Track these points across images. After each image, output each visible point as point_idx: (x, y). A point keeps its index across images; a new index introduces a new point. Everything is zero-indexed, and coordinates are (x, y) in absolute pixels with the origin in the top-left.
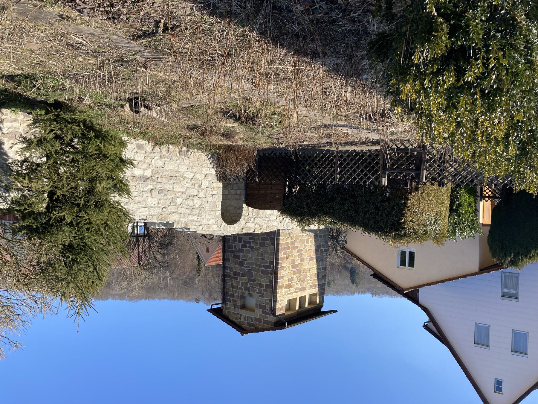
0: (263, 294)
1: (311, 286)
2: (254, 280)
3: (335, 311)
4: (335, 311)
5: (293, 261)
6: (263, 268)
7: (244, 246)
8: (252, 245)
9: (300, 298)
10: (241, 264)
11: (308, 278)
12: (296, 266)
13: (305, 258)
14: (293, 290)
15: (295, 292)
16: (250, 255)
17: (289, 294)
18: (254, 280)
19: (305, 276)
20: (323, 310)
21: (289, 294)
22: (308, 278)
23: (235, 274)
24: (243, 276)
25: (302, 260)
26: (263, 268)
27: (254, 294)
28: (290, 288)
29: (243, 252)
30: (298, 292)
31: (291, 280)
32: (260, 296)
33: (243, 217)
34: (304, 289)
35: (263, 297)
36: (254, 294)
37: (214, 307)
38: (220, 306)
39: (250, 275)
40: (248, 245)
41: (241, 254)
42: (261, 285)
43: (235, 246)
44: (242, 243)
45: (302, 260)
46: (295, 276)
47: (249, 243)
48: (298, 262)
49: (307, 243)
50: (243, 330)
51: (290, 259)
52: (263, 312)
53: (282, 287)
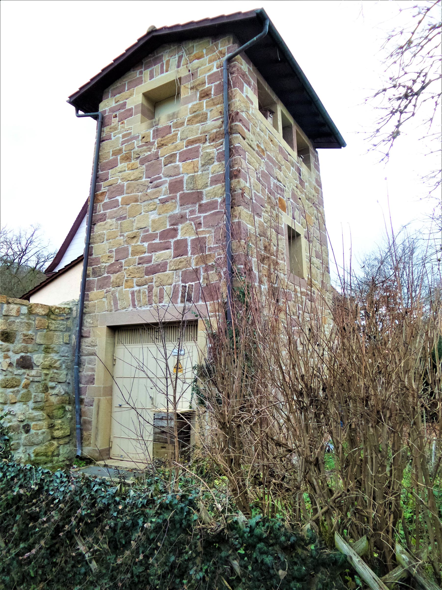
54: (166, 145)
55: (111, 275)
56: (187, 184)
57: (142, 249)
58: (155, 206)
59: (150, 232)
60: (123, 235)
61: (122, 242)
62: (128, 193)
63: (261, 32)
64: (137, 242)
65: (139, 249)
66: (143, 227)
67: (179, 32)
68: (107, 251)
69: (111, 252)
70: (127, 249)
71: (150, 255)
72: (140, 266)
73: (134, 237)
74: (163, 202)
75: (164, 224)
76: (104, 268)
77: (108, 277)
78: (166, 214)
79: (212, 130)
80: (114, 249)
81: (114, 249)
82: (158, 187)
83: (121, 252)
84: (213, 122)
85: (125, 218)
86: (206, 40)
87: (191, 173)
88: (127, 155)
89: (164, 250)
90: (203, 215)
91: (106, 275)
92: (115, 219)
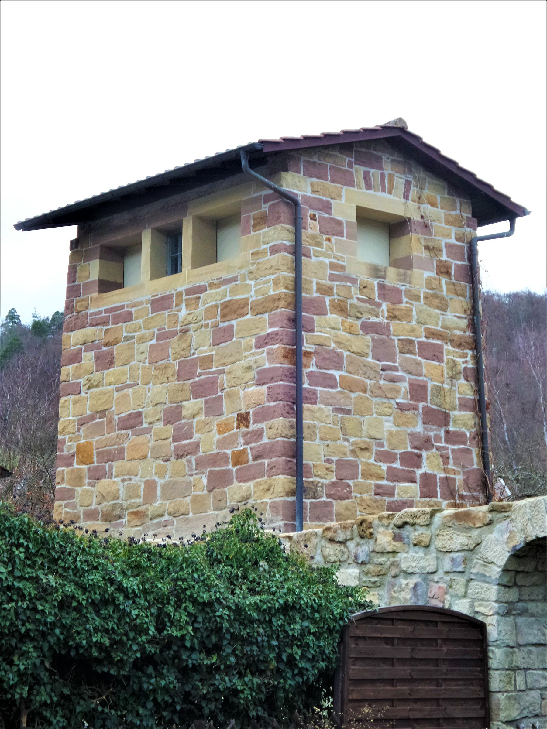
0: (332, 278)
1: (128, 317)
2: (367, 328)
3: (29, 225)
4: (29, 225)
5: (213, 408)
6: (337, 374)
7: (413, 460)
8: (384, 467)
9: (175, 267)
10: (418, 391)
11: (145, 347)
12: (198, 391)
13: (159, 425)
14: (211, 298)
15: (201, 289)
16: (388, 425)
17: (227, 281)
18: (367, 328)
19: (157, 354)
20: (71, 232)
21: (227, 281)
22: (145, 347)
23: (435, 354)
24: (407, 346)
25: (173, 416)
26: (337, 374)
27: (364, 277)
28: (226, 305)
29: (413, 435)
30: (189, 292)
31: (222, 336)
32: (343, 268)
33: (495, 572)
34: (161, 303)
35: (333, 266)
36: (364, 277)
37: (503, 226)
38: (482, 231)
39: (382, 349)
40: (397, 465)
41: (419, 428)
42: (341, 308)
43: (446, 463)
44: (419, 472)
45: (173, 416)
46: (205, 351)
47: (394, 475)
48: (191, 405)
49: (151, 486)
50: (397, 145)
51: (229, 415)
52: (327, 207)
53: (260, 308)
54: (399, 320)
55: (334, 502)
56: (432, 396)
57: (379, 472)
58: (391, 411)
59: (386, 448)
60: (347, 440)
61: (347, 450)
62: (350, 373)
63: (403, 139)
64: (370, 458)
65: (374, 470)
66: (377, 437)
67: (413, 145)
68: (323, 459)
69: (329, 461)
70: (354, 465)
71: (392, 484)
72: (378, 497)
73: (366, 449)
74: (401, 407)
75: (403, 442)
76: (322, 487)
77: (329, 505)
78: (406, 429)
79: (455, 329)
80: (335, 459)
81: (335, 459)
82: (394, 382)
83: (347, 469)
84: (455, 319)
85: (348, 412)
86: (441, 183)
87: (436, 381)
88: (342, 304)
89: (408, 482)
90: (451, 447)
91: (324, 499)
92: (331, 408)
